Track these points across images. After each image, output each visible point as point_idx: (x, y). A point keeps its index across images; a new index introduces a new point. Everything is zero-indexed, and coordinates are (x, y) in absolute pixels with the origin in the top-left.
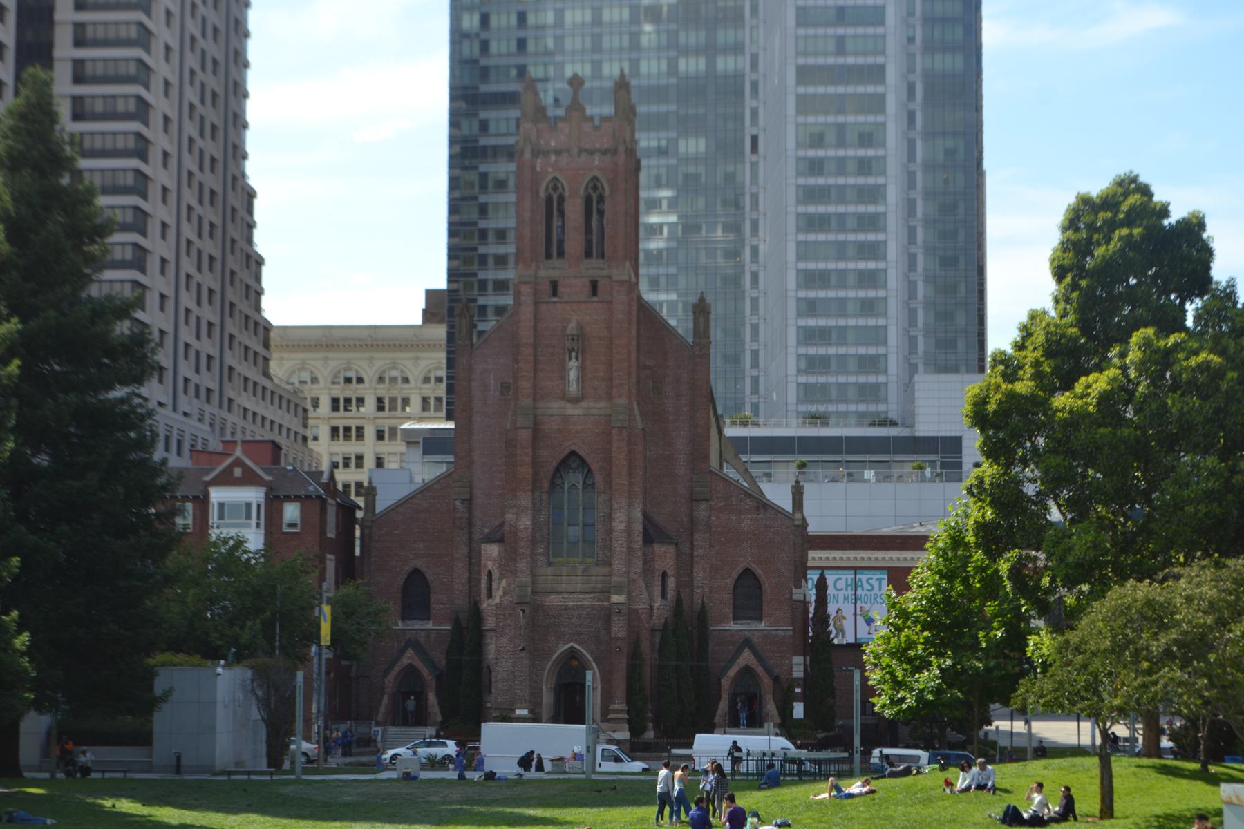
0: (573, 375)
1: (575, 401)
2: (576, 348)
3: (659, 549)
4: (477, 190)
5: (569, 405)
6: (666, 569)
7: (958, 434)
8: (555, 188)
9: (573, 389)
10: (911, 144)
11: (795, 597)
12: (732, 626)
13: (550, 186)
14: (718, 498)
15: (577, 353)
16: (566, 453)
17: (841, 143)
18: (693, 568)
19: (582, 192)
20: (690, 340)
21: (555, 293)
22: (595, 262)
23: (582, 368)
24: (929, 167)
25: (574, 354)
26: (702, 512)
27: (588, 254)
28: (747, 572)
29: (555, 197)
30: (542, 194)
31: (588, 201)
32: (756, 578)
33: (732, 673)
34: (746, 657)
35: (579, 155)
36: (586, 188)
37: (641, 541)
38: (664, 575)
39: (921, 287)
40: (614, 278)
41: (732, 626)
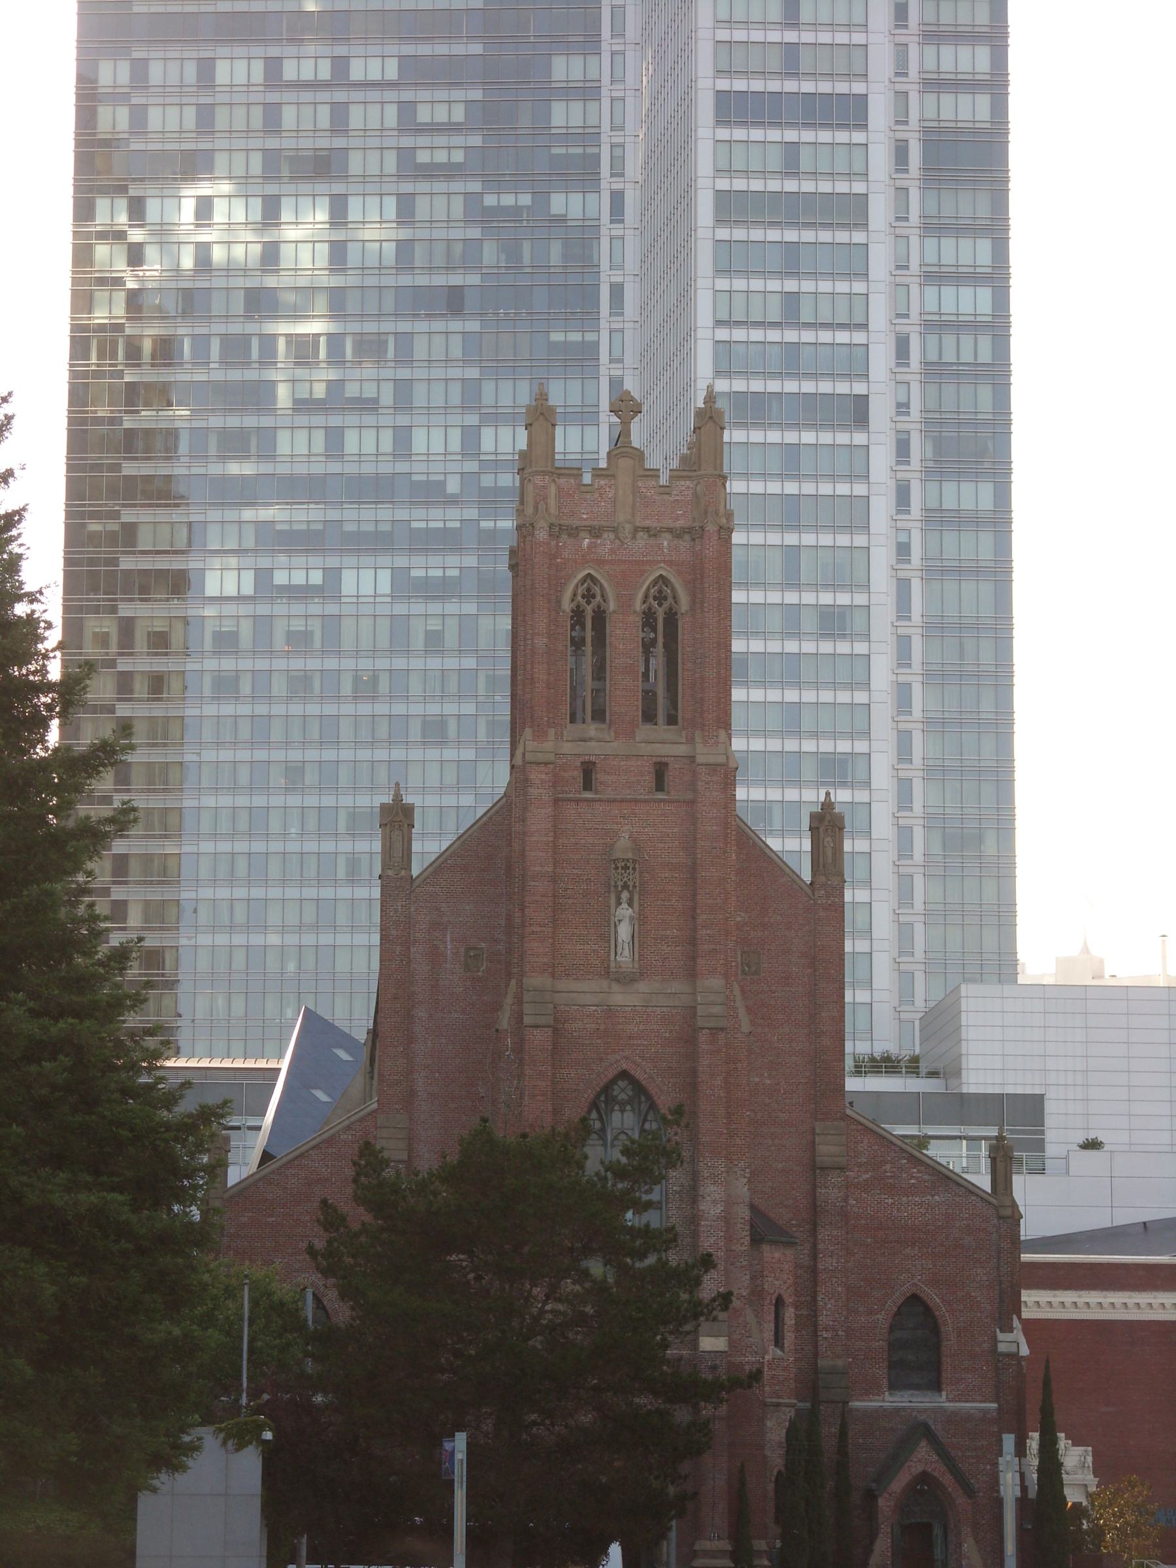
0: (624, 932)
1: (626, 980)
2: (631, 884)
3: (772, 1254)
4: (114, 649)
5: (615, 987)
6: (782, 1292)
7: (1037, 1091)
8: (589, 596)
9: (624, 957)
10: (903, 587)
11: (1002, 1348)
12: (890, 1401)
13: (580, 591)
14: (860, 1165)
15: (631, 893)
16: (611, 1074)
17: (792, 582)
18: (815, 1292)
19: (638, 606)
20: (807, 876)
21: (588, 786)
22: (662, 730)
23: (641, 920)
24: (935, 628)
25: (625, 895)
26: (831, 1191)
27: (649, 716)
28: (914, 1299)
29: (589, 611)
30: (567, 606)
31: (648, 619)
32: (928, 1311)
33: (899, 1483)
34: (923, 1458)
35: (634, 538)
36: (646, 597)
37: (748, 1238)
38: (779, 1303)
39: (918, 834)
40: (700, 759)
41: (890, 1401)
